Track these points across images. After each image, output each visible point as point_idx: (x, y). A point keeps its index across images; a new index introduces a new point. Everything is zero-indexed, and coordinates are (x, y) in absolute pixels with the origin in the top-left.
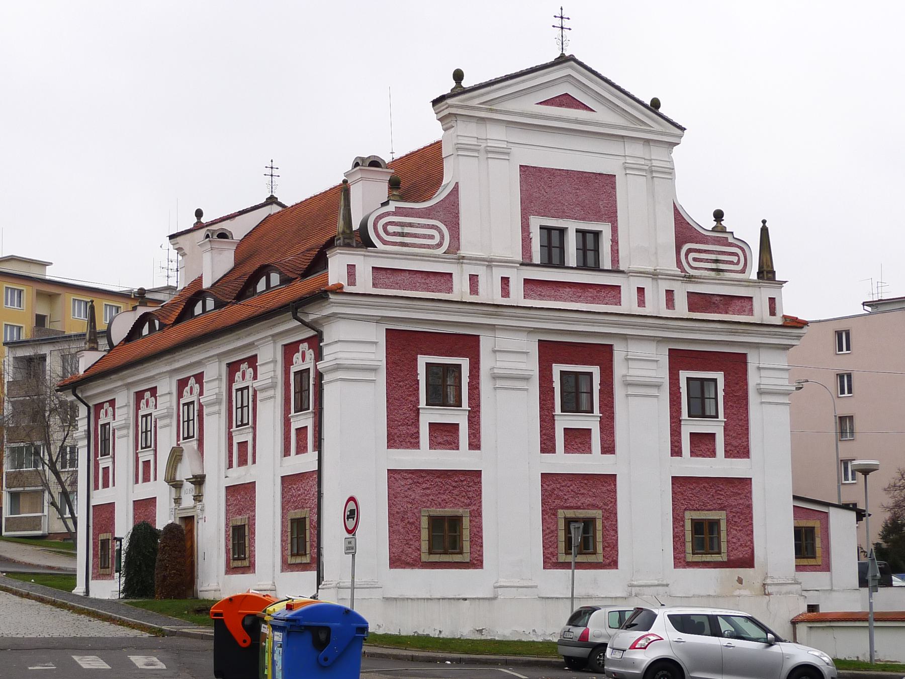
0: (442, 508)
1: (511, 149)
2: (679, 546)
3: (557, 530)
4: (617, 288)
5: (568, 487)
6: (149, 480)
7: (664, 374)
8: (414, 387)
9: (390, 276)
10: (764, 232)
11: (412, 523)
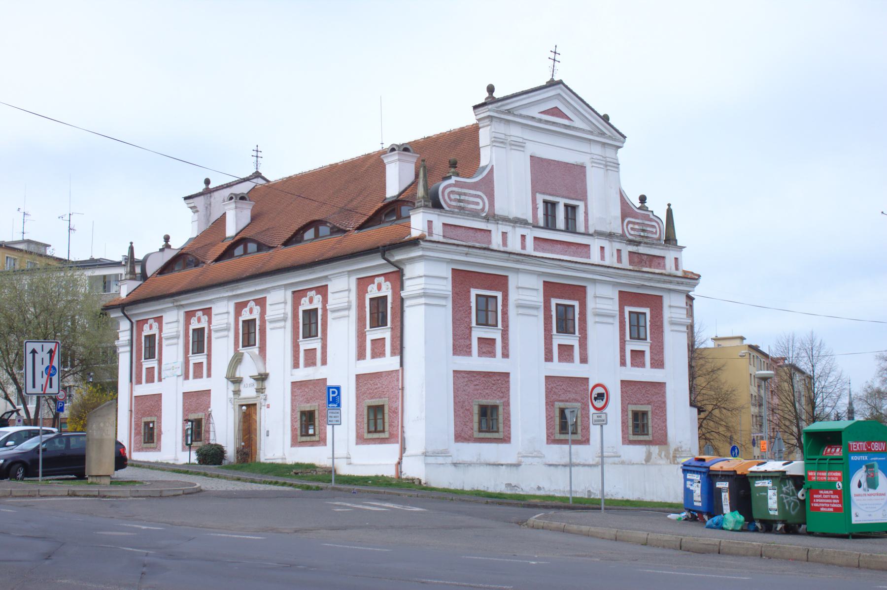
0: (486, 399)
1: (525, 143)
2: (624, 429)
3: (554, 417)
4: (588, 246)
5: (561, 386)
6: (153, 381)
7: (616, 307)
8: (469, 311)
9: (453, 231)
10: (669, 213)
11: (468, 410)
